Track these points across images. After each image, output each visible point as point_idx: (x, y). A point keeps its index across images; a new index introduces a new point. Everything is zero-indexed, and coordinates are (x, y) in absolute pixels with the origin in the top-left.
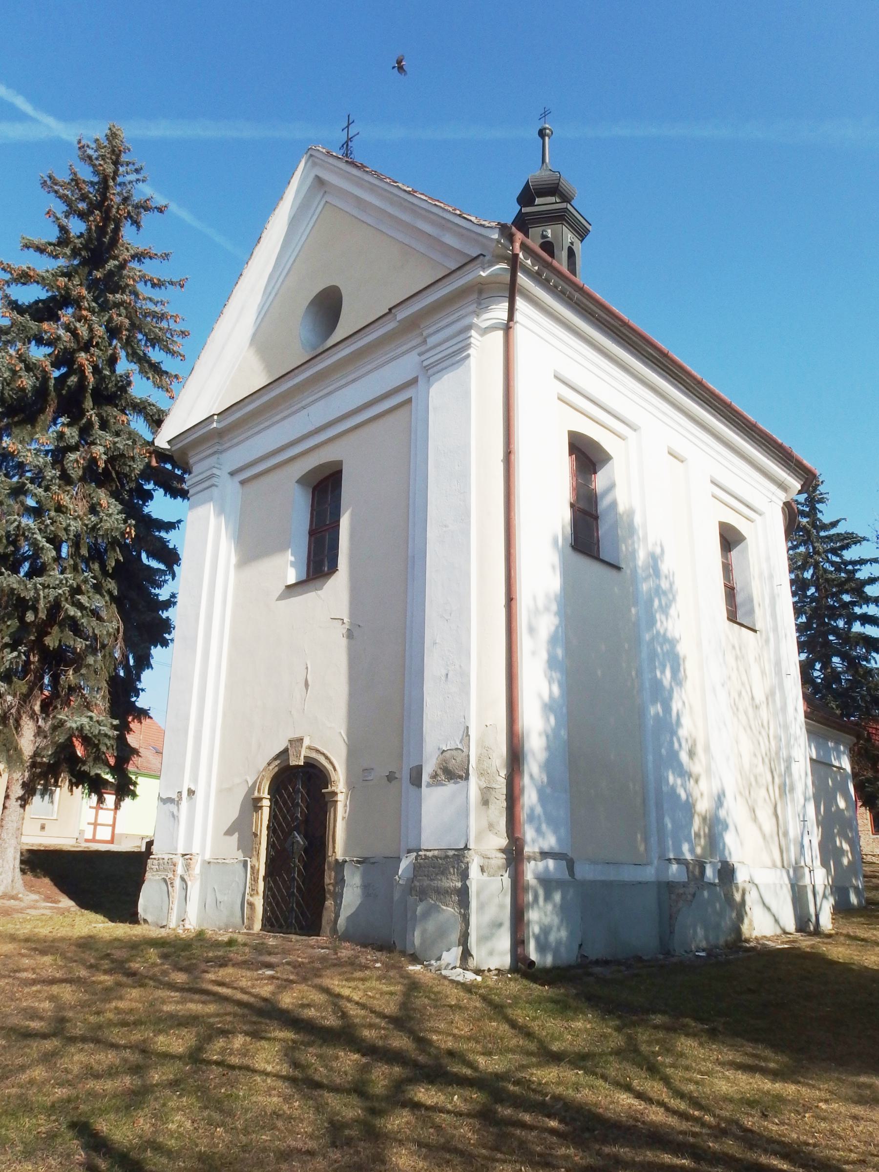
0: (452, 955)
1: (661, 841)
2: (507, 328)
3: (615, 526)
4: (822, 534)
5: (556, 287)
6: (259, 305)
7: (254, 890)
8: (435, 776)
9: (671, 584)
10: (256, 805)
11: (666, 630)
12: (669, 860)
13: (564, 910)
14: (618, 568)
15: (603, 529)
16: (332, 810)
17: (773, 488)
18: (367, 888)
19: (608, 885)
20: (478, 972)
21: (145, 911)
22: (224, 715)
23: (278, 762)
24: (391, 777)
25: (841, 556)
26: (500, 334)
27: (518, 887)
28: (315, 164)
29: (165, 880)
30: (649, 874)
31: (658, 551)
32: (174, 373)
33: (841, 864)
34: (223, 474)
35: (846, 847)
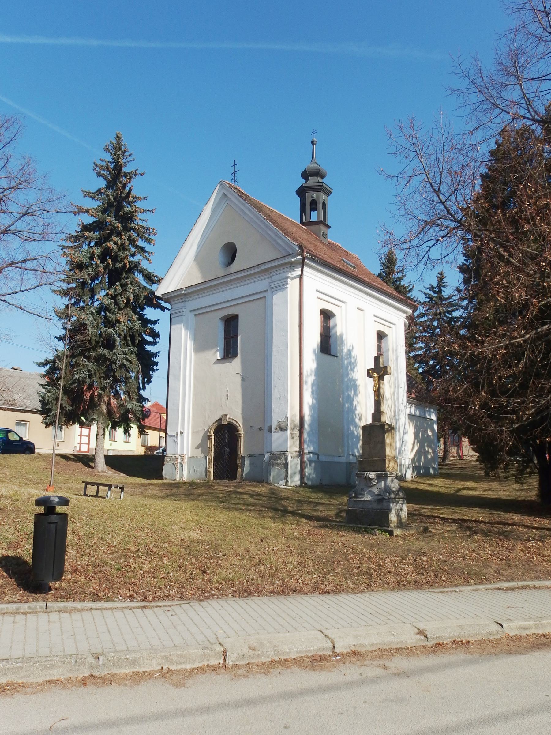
0: (283, 482)
1: (348, 450)
2: (301, 277)
3: (336, 340)
4: (444, 302)
5: (317, 261)
6: (199, 242)
7: (210, 467)
8: (276, 429)
9: (355, 360)
10: (209, 437)
11: (353, 377)
12: (350, 455)
13: (315, 469)
14: (337, 357)
15: (332, 340)
17: (400, 313)
18: (251, 464)
19: (330, 463)
20: (291, 486)
21: (165, 475)
22: (193, 405)
23: (217, 423)
24: (260, 429)
25: (451, 315)
26: (298, 280)
27: (302, 463)
28: (223, 188)
29: (174, 464)
30: (343, 459)
31: (351, 348)
32: (151, 251)
33: (428, 458)
34: (186, 311)
35: (430, 450)
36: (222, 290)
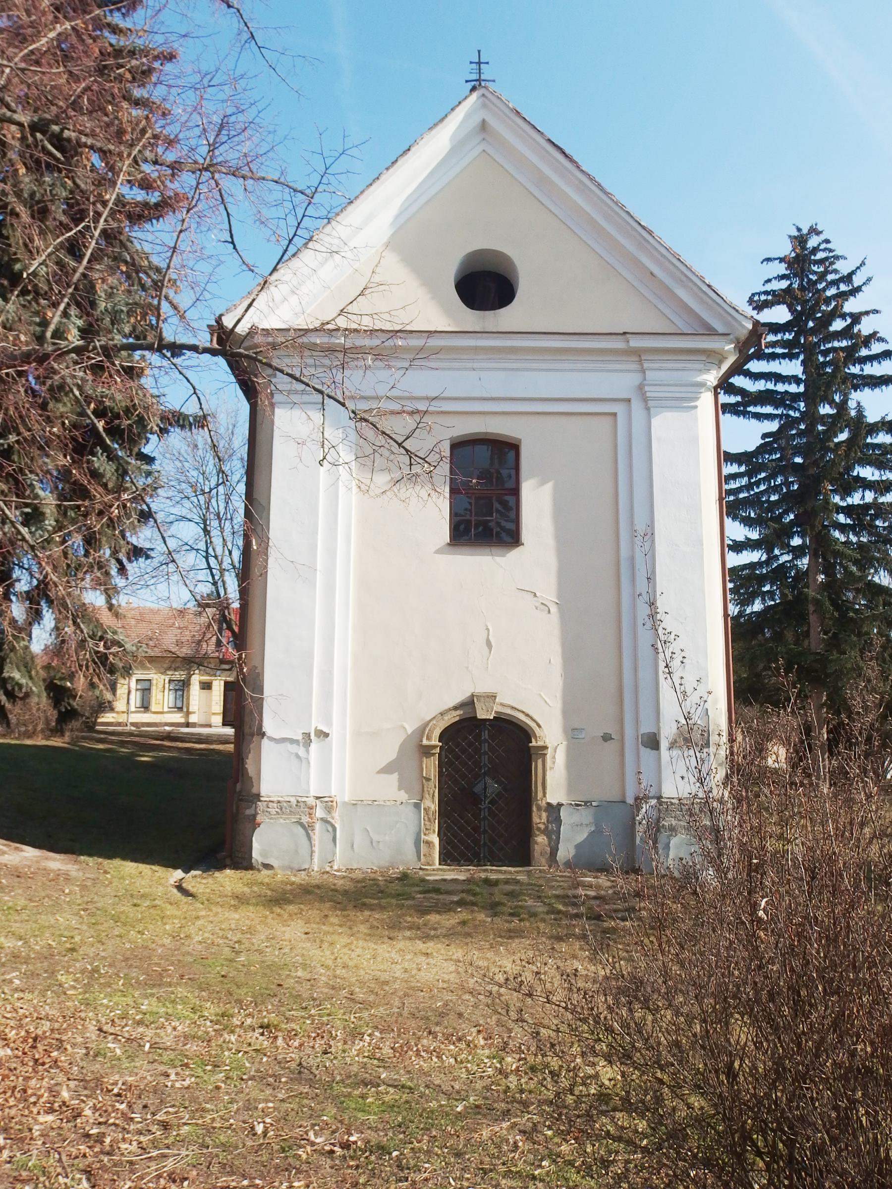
16: (540, 762)
28: (484, 106)
36: (476, 365)
